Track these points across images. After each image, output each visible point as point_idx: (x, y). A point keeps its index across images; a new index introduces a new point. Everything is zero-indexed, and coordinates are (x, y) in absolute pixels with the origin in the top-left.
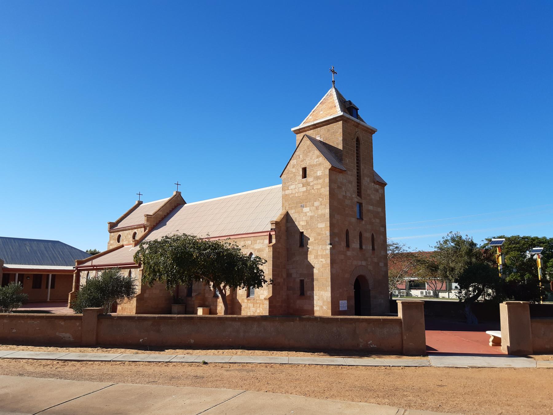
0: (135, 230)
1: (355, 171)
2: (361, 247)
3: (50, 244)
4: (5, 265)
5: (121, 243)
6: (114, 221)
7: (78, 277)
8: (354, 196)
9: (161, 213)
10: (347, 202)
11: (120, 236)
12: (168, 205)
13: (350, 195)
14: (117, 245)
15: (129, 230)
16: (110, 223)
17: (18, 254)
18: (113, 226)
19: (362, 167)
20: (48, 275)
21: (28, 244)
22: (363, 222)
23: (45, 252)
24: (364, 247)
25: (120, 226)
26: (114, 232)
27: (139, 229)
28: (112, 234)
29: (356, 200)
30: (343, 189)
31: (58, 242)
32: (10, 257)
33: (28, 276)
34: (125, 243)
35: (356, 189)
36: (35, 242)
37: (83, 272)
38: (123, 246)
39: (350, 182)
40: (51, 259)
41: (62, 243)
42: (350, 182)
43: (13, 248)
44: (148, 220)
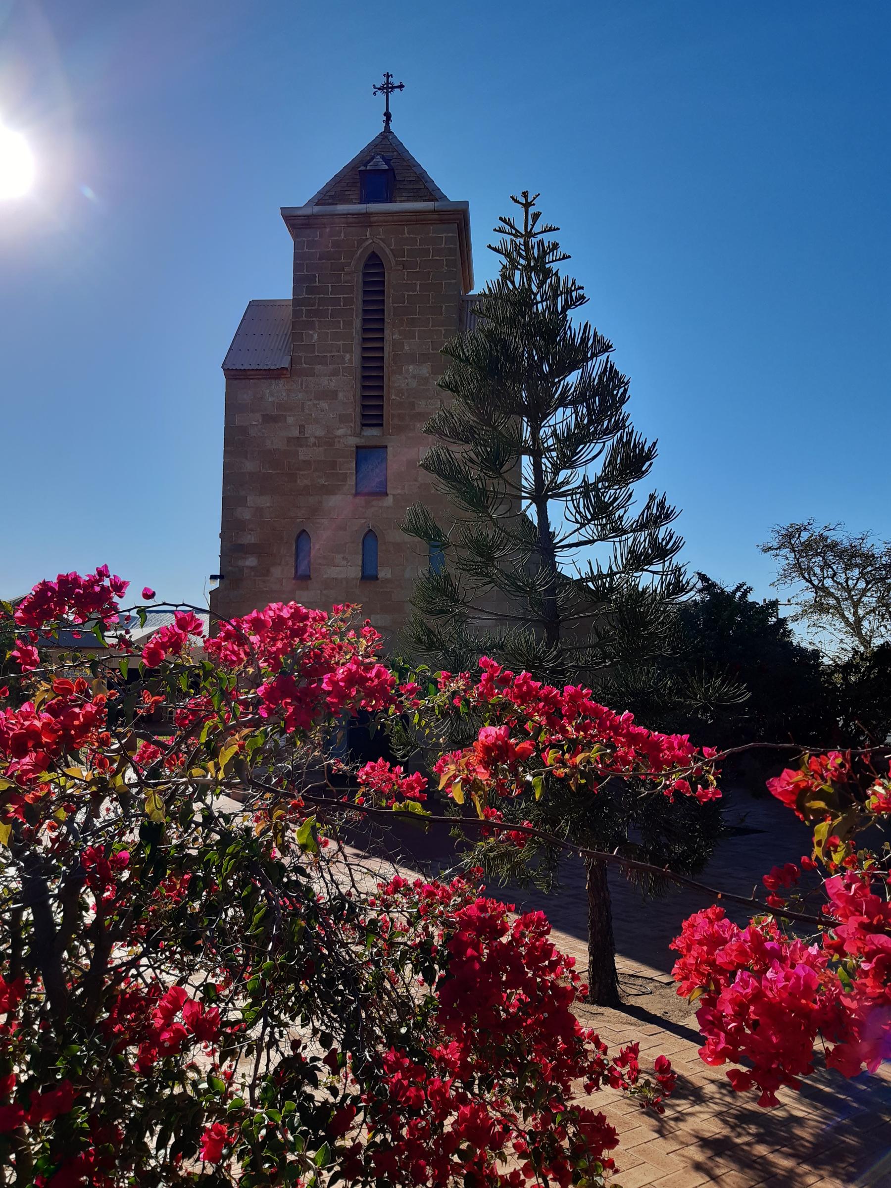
1: (353, 358)
2: (369, 577)
8: (340, 432)
10: (304, 454)
13: (320, 432)
19: (391, 335)
22: (389, 501)
24: (384, 573)
29: (353, 441)
30: (290, 420)
35: (354, 411)
39: (332, 395)
42: (332, 395)
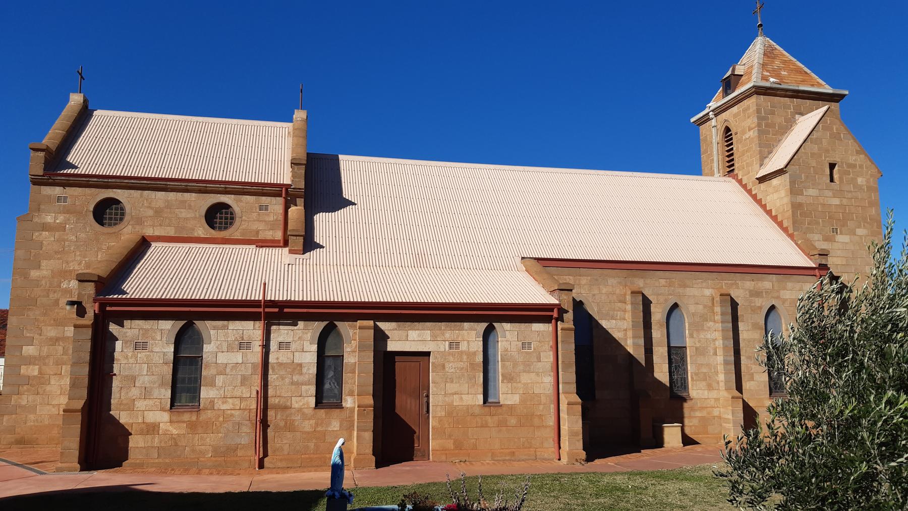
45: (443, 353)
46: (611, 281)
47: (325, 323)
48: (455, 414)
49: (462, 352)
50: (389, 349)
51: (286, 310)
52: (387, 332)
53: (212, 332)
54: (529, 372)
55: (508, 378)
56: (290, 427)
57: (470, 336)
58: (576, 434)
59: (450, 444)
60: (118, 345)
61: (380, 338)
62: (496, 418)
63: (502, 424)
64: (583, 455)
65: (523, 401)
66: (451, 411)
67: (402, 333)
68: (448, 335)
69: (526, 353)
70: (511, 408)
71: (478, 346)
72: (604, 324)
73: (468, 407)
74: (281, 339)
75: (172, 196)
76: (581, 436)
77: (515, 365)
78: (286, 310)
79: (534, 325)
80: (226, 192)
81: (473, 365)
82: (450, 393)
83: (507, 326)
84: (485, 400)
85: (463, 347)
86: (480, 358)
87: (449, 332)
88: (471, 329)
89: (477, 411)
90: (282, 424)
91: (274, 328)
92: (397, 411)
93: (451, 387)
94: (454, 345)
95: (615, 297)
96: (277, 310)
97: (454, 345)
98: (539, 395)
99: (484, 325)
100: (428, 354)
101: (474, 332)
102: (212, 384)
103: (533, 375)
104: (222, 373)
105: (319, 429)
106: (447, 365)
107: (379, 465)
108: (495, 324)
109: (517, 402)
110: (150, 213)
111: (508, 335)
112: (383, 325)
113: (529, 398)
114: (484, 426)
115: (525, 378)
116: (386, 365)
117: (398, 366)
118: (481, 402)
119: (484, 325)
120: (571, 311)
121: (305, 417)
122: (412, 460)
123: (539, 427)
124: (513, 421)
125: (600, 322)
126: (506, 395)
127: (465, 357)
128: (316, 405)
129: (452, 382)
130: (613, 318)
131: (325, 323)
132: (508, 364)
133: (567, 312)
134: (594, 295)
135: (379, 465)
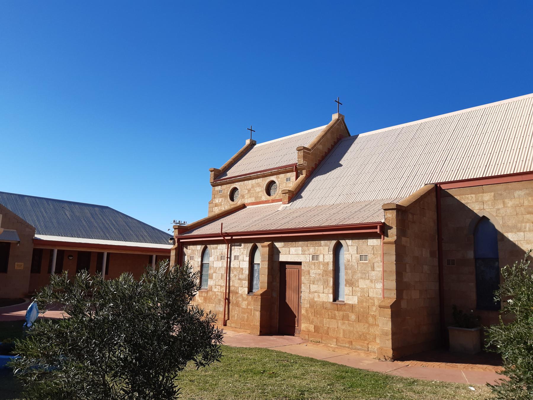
0: (273, 178)
3: (96, 209)
4: (37, 236)
5: (238, 202)
6: (220, 167)
7: (180, 255)
9: (320, 147)
11: (235, 190)
12: (329, 135)
14: (227, 205)
15: (258, 177)
16: (214, 170)
17: (54, 221)
18: (219, 177)
20: (52, 251)
21: (68, 208)
23: (93, 220)
25: (230, 173)
26: (221, 184)
27: (282, 176)
28: (218, 188)
31: (107, 207)
32: (42, 224)
33: (70, 254)
34: (246, 201)
36: (77, 206)
37: (191, 247)
38: (244, 206)
40: (102, 230)
41: (113, 210)
43: (46, 212)
44: (305, 157)
45: (308, 263)
46: (517, 193)
47: (252, 244)
48: (315, 307)
49: (320, 262)
50: (280, 260)
51: (234, 238)
52: (279, 249)
53: (213, 250)
54: (365, 279)
55: (350, 283)
56: (238, 305)
57: (325, 250)
58: (386, 334)
59: (312, 328)
60: (186, 257)
61: (274, 253)
62: (341, 313)
63: (345, 318)
64: (390, 353)
65: (360, 301)
66: (312, 304)
67: (287, 249)
68: (312, 250)
69: (363, 263)
70: (352, 306)
71: (329, 258)
72: (511, 236)
73: (323, 303)
74: (235, 254)
75: (254, 181)
76: (390, 337)
77: (354, 273)
78: (234, 238)
79: (369, 240)
80: (272, 174)
81: (325, 271)
82: (311, 292)
83: (349, 242)
84: (336, 297)
85: (321, 258)
86: (331, 267)
87: (311, 248)
88: (326, 245)
89: (329, 306)
90: (235, 302)
91: (233, 247)
92: (287, 301)
93: (314, 288)
94: (315, 257)
95: (522, 209)
96: (230, 238)
97: (315, 257)
98: (373, 299)
99: (334, 242)
100: (300, 263)
101: (327, 248)
102: (212, 278)
103: (368, 282)
104: (215, 272)
105: (249, 307)
106: (311, 272)
107: (262, 333)
108: (342, 242)
109: (356, 302)
110: (247, 191)
111: (350, 249)
112: (278, 245)
113: (365, 298)
114: (334, 317)
115: (363, 284)
116: (279, 271)
117: (288, 271)
118: (331, 300)
119: (334, 242)
120: (395, 228)
121: (243, 299)
122: (294, 335)
123: (372, 325)
124: (353, 317)
125: (506, 235)
126: (347, 295)
127: (321, 266)
128: (248, 293)
129: (314, 284)
130: (520, 230)
131: (252, 244)
132: (350, 272)
133: (391, 228)
134: (498, 209)
135: (262, 333)
